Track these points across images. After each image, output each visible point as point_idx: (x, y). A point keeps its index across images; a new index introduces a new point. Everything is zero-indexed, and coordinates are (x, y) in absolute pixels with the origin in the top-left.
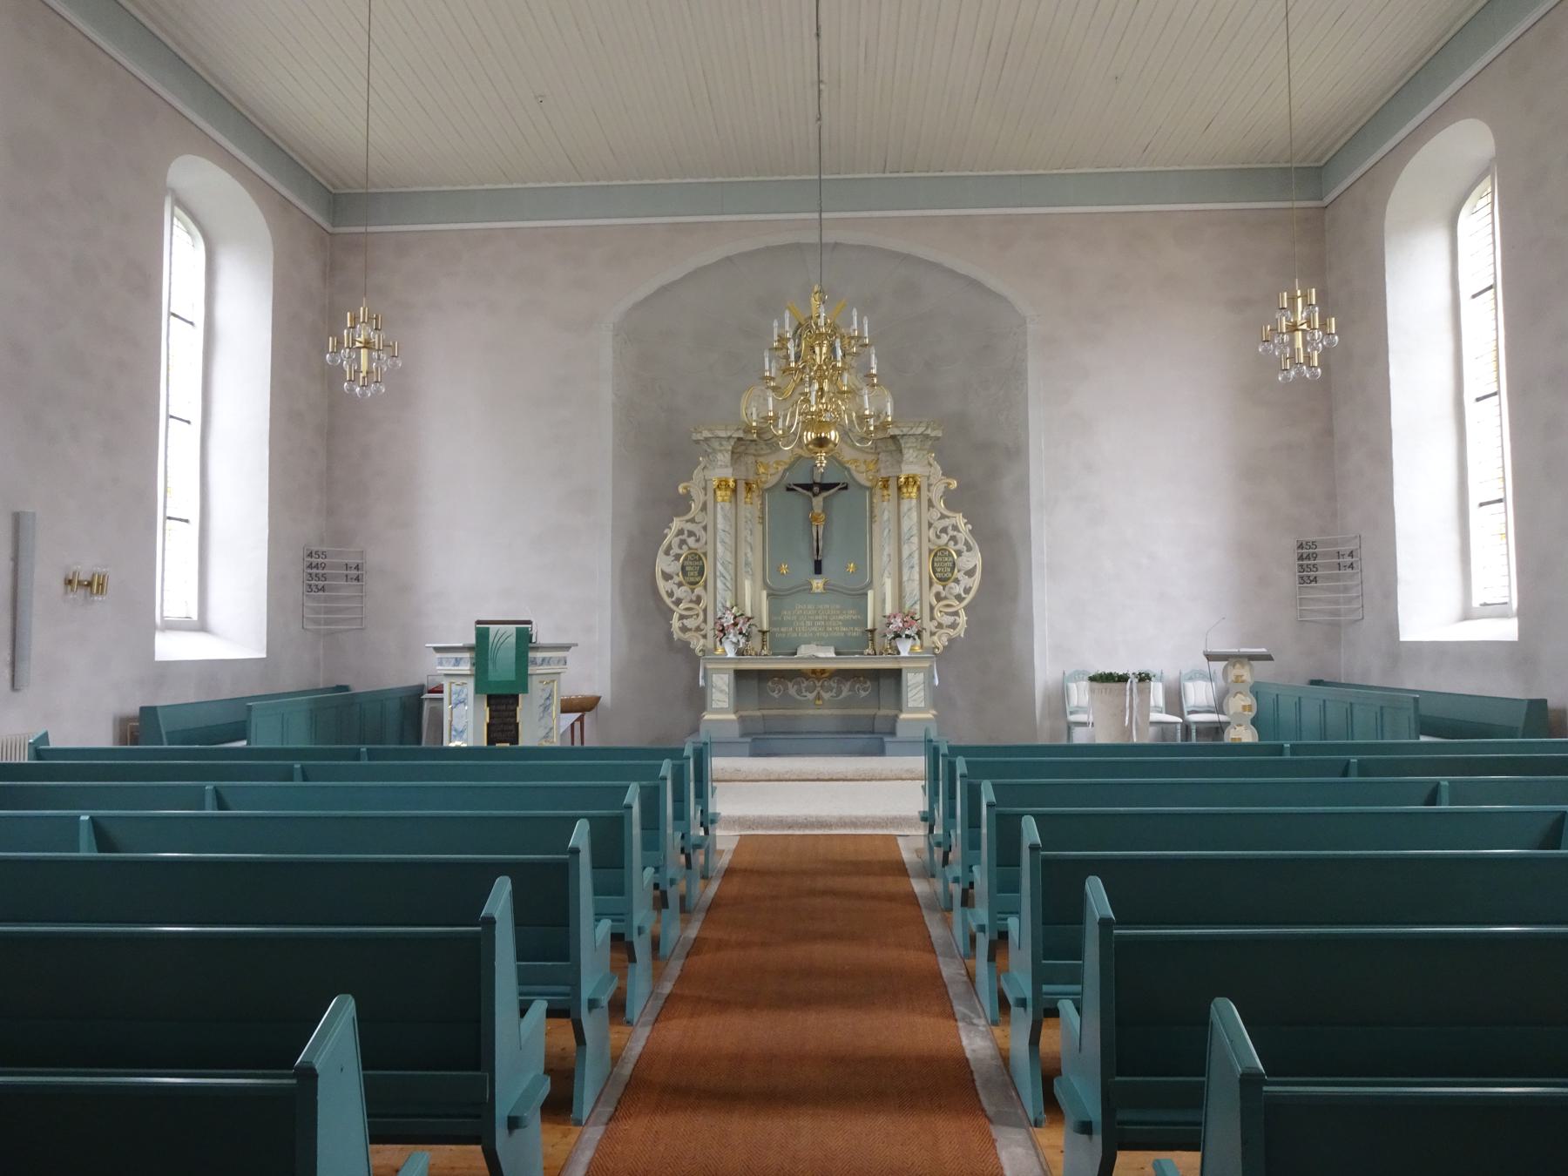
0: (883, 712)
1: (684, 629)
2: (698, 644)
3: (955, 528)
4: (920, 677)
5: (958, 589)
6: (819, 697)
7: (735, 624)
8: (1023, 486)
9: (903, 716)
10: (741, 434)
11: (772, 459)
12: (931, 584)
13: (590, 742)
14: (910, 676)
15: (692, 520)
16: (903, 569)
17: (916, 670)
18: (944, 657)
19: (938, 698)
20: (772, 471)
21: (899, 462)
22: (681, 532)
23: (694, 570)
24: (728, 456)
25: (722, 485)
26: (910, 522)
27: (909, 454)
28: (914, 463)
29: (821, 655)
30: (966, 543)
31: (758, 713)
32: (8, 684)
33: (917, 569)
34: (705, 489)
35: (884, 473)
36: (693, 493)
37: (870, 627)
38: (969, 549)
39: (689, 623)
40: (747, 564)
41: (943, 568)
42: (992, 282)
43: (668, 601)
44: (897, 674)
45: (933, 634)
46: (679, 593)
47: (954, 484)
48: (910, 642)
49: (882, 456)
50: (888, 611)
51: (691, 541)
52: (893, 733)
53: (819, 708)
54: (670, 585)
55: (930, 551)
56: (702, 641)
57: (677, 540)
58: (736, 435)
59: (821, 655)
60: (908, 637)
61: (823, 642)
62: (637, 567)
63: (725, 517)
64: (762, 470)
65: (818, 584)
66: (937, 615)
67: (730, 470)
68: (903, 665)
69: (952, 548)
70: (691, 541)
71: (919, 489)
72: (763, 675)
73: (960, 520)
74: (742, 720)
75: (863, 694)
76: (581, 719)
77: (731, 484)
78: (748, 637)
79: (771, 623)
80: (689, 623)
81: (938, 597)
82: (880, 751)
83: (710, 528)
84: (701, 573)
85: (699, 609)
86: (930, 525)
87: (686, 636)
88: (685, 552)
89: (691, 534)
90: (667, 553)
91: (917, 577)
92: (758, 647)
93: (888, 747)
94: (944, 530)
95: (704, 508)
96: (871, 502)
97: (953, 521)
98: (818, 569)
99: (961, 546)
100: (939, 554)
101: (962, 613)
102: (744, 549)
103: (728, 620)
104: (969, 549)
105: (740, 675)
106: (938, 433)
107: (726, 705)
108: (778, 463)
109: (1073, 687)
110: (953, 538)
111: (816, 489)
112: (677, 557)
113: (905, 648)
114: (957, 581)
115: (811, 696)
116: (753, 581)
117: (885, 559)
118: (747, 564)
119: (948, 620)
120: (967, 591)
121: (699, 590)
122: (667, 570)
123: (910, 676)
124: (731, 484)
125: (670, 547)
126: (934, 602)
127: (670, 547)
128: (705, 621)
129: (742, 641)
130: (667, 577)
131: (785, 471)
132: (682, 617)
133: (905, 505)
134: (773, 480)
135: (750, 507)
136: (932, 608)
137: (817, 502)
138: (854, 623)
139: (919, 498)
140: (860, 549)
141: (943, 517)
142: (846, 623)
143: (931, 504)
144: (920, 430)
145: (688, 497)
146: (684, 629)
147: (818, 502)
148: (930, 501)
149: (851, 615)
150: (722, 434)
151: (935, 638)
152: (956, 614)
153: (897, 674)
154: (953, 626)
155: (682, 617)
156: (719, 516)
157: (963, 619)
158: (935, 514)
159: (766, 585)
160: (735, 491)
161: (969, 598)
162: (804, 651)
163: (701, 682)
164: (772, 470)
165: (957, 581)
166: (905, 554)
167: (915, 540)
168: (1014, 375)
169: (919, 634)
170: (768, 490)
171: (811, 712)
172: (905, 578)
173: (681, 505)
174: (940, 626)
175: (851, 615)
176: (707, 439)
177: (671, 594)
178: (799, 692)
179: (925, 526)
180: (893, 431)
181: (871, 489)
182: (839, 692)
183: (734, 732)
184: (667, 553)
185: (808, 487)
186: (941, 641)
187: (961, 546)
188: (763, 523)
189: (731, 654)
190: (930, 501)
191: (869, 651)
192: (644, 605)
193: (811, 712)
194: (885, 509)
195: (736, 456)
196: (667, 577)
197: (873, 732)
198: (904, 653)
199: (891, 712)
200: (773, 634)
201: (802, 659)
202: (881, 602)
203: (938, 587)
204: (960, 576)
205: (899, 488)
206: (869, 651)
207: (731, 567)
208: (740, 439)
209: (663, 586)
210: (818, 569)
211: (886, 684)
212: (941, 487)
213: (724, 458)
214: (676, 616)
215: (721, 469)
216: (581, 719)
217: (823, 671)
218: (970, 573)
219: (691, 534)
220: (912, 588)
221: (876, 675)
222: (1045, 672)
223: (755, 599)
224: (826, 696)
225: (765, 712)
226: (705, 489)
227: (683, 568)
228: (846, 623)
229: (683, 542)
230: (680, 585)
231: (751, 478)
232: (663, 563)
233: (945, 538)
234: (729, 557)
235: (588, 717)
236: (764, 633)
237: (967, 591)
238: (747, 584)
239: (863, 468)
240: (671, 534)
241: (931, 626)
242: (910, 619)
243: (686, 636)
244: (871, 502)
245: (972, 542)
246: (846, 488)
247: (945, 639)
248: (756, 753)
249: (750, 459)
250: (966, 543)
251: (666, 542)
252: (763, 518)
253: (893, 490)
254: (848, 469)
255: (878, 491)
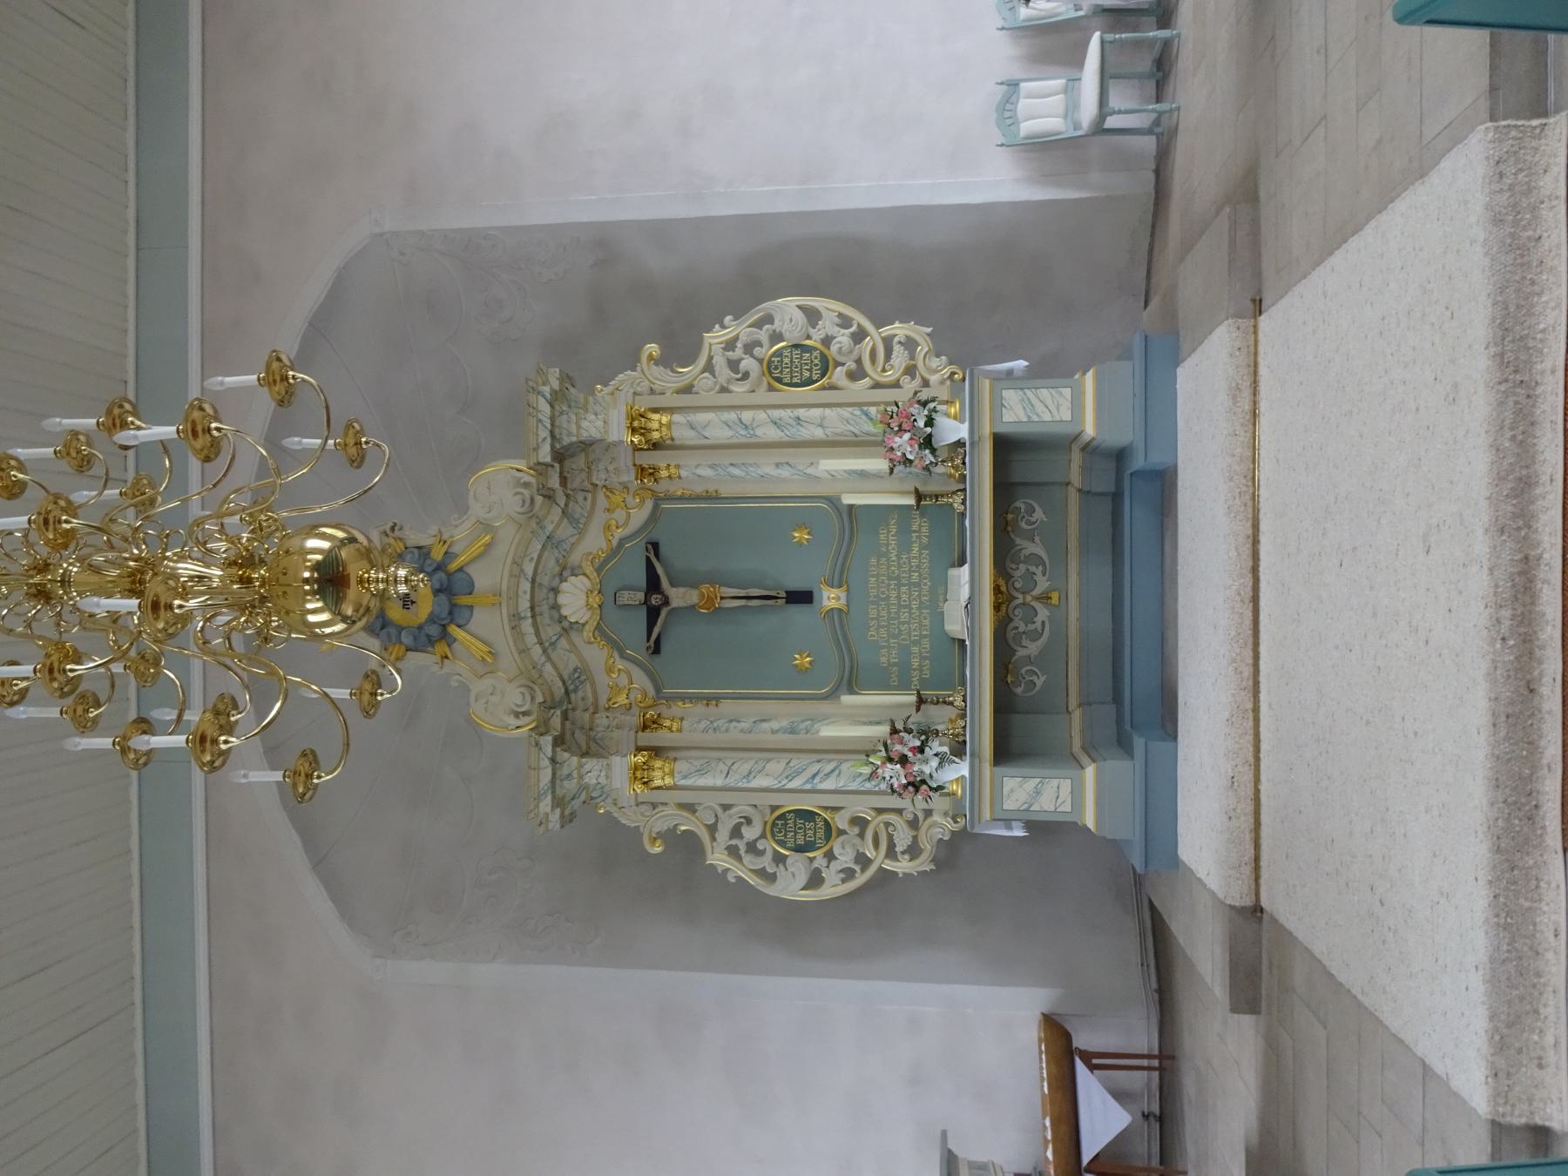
0: (1075, 477)
1: (913, 851)
2: (941, 826)
3: (730, 345)
4: (1010, 396)
5: (843, 338)
6: (1045, 598)
7: (903, 760)
8: (661, 232)
9: (1090, 430)
10: (547, 742)
11: (603, 680)
12: (833, 387)
13: (1142, 1038)
14: (1008, 417)
15: (712, 829)
16: (796, 441)
17: (998, 405)
18: (965, 354)
19: (1047, 370)
20: (624, 681)
21: (609, 447)
22: (733, 851)
23: (802, 829)
24: (590, 763)
25: (640, 775)
26: (717, 427)
27: (590, 427)
28: (605, 420)
29: (965, 592)
30: (758, 324)
31: (1077, 715)
32: (949, 1135)
33: (801, 412)
34: (654, 806)
35: (629, 476)
36: (661, 826)
37: (911, 501)
38: (769, 319)
39: (903, 840)
40: (792, 731)
41: (804, 367)
42: (313, 292)
43: (861, 879)
44: (1005, 447)
45: (926, 383)
46: (845, 858)
47: (653, 348)
48: (940, 420)
49: (599, 478)
50: (879, 464)
51: (750, 833)
52: (1120, 456)
53: (1069, 597)
54: (831, 875)
55: (771, 389)
56: (937, 818)
57: (748, 859)
58: (549, 750)
59: (966, 590)
60: (930, 422)
61: (940, 589)
62: (796, 932)
63: (700, 772)
64: (622, 699)
65: (831, 598)
66: (890, 376)
67: (616, 760)
68: (987, 431)
69: (766, 352)
70: (750, 833)
71: (655, 410)
72: (1004, 705)
73: (715, 338)
74: (1092, 750)
75: (1039, 514)
76: (1087, 1057)
77: (640, 759)
78: (927, 734)
79: (903, 686)
80: (903, 840)
81: (856, 375)
82: (1163, 483)
83: (727, 798)
84: (808, 816)
85: (876, 822)
86: (724, 390)
87: (927, 847)
88: (769, 845)
89: (736, 832)
90: (772, 878)
91: (816, 412)
92: (951, 712)
93: (1157, 459)
94: (733, 365)
95: (690, 808)
96: (681, 499)
97: (717, 349)
98: (802, 597)
99: (763, 335)
100: (775, 373)
101: (886, 330)
102: (767, 733)
103: (893, 772)
104: (769, 319)
105: (1004, 752)
106: (554, 374)
107: (1066, 785)
108: (610, 670)
109: (1027, 127)
110: (749, 349)
111: (655, 600)
112: (779, 859)
113: (952, 429)
114: (827, 341)
115: (1043, 613)
116: (824, 718)
117: (785, 472)
118: (792, 731)
119: (900, 358)
120: (845, 322)
121: (841, 821)
122: (803, 879)
123: (1008, 417)
124: (640, 759)
125: (761, 873)
126: (866, 382)
127: (761, 873)
128: (899, 811)
129: (936, 746)
130: (815, 880)
131: (623, 656)
132: (891, 853)
133: (683, 435)
134: (641, 681)
135: (688, 723)
136: (877, 385)
137: (683, 598)
138: (904, 530)
139: (671, 410)
140: (766, 519)
141: (709, 368)
142: (905, 547)
143: (688, 390)
144: (544, 407)
145: (671, 837)
146: (913, 851)
147: (679, 597)
148: (679, 392)
149: (888, 537)
150: (546, 776)
151: (934, 379)
152: (888, 342)
153: (1005, 447)
154: (910, 344)
155: (891, 853)
156: (701, 782)
157: (899, 330)
158: (706, 380)
159: (833, 695)
160: (656, 751)
161: (859, 318)
162: (956, 625)
163: (1019, 832)
164: (618, 679)
165: (827, 341)
166: (773, 434)
167: (747, 416)
168: (475, 254)
169: (924, 404)
170: (658, 690)
171: (1073, 615)
172: (819, 433)
173: (686, 847)
174: (910, 371)
175: (888, 537)
176: (558, 802)
177: (849, 874)
178: (1035, 635)
179: (724, 399)
180: (545, 454)
181: (658, 501)
182: (1036, 559)
183: (1124, 770)
184: (772, 878)
185: (653, 614)
186: (938, 370)
187: (763, 335)
188: (718, 699)
189: (962, 769)
190: (679, 392)
191: (958, 499)
192: (869, 921)
193: (1073, 615)
194: (695, 473)
195: (593, 748)
196: (815, 880)
197: (1117, 497)
198: (962, 431)
199: (1076, 457)
200: (924, 683)
201: (972, 630)
202: (864, 479)
203: (838, 375)
204: (817, 336)
205: (656, 446)
206: (958, 507)
207: (797, 762)
208: (559, 742)
209: (832, 888)
210: (802, 597)
211: (1022, 470)
212: (657, 371)
213: (593, 771)
214: (889, 865)
215: (613, 775)
216: (1087, 1057)
217: (997, 590)
218: (813, 316)
219: (736, 832)
220: (837, 421)
221: (1004, 490)
222: (1000, 182)
223: (857, 719)
224: (1042, 585)
225: (1073, 702)
226: (654, 806)
227: (799, 849)
228: (905, 547)
229: (752, 848)
230: (830, 856)
231: (635, 719)
232: (791, 886)
233: (748, 363)
234: (777, 766)
235: (1081, 1041)
236: (921, 701)
237: (845, 322)
238: (828, 731)
239: (620, 515)
240: (739, 871)
241: (910, 385)
242: (895, 421)
243: (927, 847)
244: (681, 499)
245: (755, 316)
246: (655, 546)
247: (935, 362)
248: (1164, 716)
249: (602, 720)
250: (758, 324)
251: (753, 880)
252: (708, 699)
253: (658, 459)
254: (622, 542)
255: (662, 487)
